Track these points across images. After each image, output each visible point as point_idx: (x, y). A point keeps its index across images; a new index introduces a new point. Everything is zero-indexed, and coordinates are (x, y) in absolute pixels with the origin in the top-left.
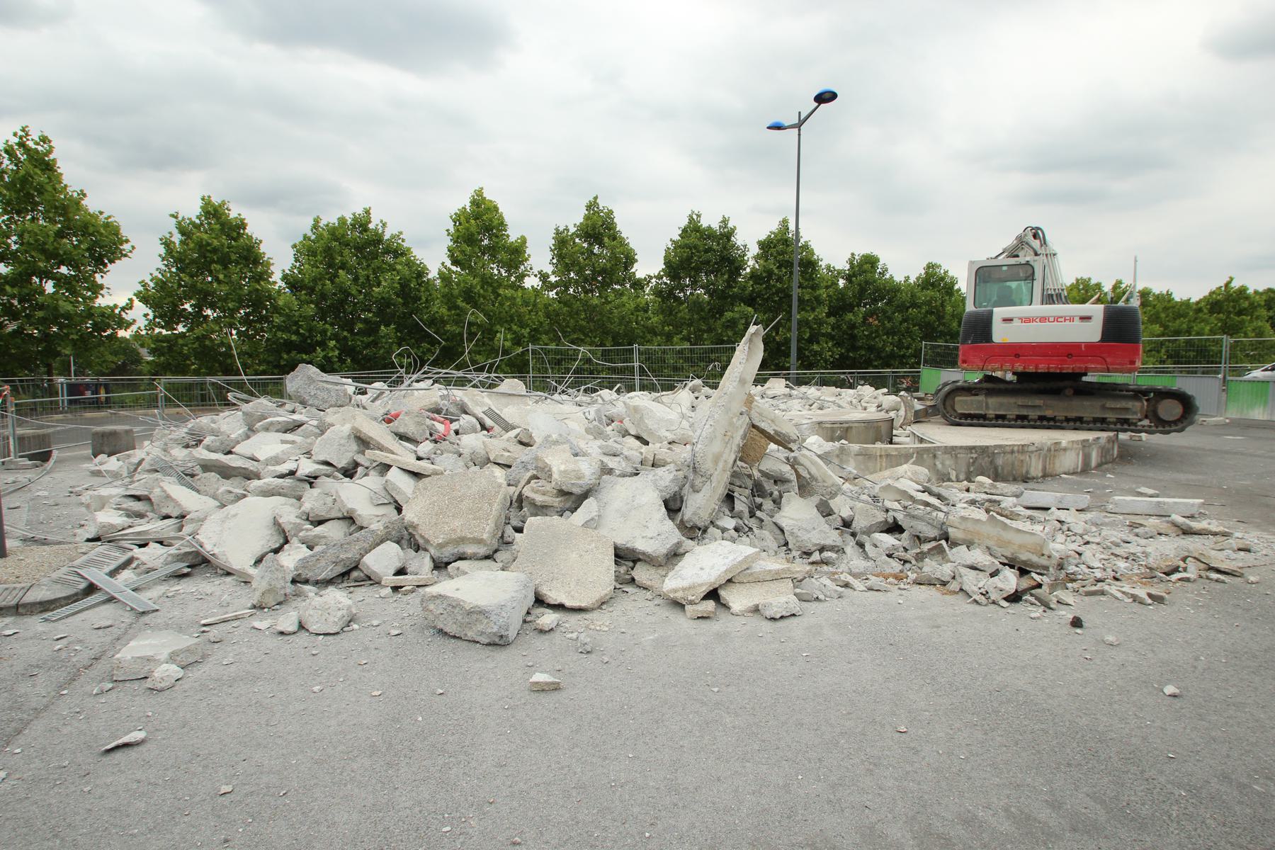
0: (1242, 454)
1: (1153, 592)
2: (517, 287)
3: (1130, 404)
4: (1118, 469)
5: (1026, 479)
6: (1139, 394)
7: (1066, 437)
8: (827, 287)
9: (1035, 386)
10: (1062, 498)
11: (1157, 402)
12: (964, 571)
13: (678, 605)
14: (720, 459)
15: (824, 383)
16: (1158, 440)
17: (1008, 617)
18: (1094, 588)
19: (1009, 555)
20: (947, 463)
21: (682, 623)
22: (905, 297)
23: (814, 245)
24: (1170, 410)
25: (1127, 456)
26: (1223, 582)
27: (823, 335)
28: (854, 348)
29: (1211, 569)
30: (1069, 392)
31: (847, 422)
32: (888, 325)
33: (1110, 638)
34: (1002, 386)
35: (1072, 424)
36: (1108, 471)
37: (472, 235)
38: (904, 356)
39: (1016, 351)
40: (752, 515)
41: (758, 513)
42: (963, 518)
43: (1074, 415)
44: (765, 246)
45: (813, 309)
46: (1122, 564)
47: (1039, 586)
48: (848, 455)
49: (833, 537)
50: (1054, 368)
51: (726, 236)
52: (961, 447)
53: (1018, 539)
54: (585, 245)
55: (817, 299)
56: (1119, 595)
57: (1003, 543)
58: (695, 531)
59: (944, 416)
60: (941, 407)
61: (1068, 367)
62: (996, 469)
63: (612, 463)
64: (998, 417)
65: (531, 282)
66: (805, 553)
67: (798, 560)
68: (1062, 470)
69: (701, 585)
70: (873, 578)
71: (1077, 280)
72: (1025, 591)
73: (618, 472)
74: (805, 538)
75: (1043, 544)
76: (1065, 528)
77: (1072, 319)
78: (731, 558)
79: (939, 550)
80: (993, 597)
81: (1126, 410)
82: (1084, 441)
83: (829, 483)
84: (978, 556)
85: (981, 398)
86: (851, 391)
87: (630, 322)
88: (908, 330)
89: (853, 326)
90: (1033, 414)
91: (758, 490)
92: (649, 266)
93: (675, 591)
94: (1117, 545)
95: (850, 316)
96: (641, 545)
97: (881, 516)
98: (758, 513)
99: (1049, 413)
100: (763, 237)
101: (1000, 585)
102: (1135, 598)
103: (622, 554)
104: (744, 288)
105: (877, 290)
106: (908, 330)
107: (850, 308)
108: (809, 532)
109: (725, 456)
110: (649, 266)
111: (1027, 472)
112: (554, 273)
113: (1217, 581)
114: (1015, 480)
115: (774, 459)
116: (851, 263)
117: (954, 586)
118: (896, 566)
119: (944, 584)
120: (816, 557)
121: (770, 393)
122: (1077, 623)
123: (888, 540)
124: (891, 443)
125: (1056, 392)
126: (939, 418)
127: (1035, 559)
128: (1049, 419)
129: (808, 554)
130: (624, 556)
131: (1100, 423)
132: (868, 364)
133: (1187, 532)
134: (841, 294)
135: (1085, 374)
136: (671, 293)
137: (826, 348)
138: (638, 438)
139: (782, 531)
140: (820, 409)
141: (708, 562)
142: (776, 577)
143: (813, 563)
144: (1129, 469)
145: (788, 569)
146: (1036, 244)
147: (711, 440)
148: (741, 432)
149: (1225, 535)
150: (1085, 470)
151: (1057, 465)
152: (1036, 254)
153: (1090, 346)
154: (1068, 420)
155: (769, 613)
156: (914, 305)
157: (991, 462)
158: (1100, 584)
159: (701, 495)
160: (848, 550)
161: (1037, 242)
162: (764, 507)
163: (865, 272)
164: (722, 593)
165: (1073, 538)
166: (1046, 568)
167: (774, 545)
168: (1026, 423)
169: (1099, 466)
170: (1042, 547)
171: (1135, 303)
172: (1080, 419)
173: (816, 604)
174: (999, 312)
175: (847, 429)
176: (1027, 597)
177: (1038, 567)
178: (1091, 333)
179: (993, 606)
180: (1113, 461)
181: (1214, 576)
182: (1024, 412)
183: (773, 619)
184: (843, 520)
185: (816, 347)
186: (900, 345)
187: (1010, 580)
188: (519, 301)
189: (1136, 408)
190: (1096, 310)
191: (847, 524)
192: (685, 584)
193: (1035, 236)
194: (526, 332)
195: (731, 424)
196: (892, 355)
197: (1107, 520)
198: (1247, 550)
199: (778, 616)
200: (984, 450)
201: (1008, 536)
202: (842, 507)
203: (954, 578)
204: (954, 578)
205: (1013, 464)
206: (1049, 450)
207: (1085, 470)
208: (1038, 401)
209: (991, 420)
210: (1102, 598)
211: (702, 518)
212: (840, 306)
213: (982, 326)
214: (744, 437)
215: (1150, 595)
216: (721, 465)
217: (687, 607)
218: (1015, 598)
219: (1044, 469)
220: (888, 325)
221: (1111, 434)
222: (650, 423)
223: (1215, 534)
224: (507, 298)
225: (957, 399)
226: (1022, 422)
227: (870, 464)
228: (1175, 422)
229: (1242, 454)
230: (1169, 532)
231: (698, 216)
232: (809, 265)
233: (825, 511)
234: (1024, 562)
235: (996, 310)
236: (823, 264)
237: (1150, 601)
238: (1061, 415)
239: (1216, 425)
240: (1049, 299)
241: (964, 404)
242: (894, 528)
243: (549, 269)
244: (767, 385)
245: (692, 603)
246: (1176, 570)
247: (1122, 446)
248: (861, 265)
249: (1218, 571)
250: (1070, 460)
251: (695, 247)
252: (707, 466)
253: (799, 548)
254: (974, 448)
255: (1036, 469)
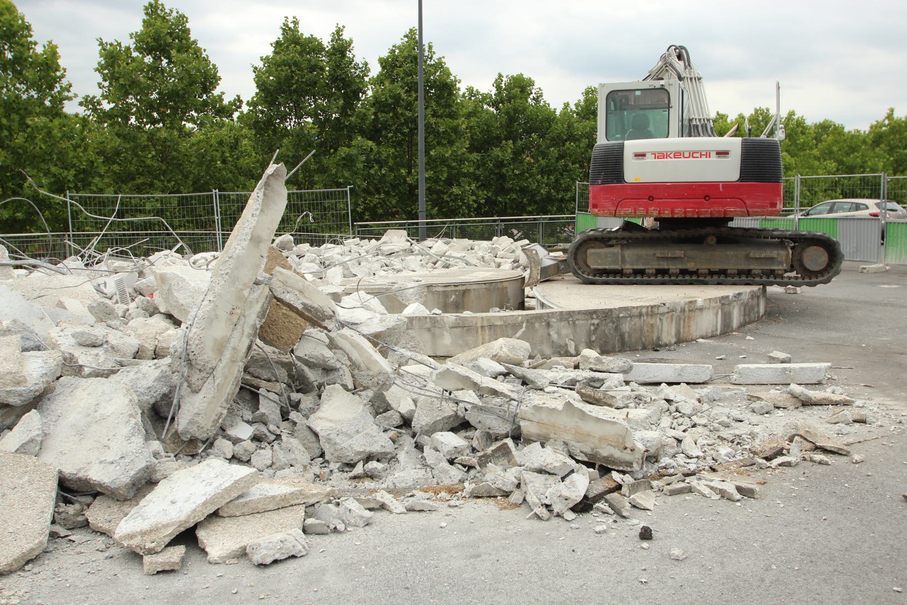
0: (893, 305)
1: (744, 484)
2: (55, 112)
3: (774, 253)
4: (763, 329)
5: (657, 347)
6: (782, 241)
7: (702, 294)
8: (469, 115)
9: (675, 234)
10: (682, 370)
11: (803, 249)
12: (529, 476)
13: (135, 556)
14: (227, 343)
15: (464, 234)
16: (804, 291)
17: (569, 534)
18: (682, 485)
19: (588, 451)
20: (564, 332)
21: (135, 581)
22: (558, 128)
23: (449, 64)
24: (815, 258)
25: (776, 313)
26: (827, 464)
27: (465, 175)
28: (502, 191)
29: (817, 448)
30: (712, 240)
31: (463, 284)
32: (543, 162)
33: (676, 552)
34: (638, 235)
35: (715, 277)
36: (750, 332)
37: (190, 48)
38: (562, 200)
39: (650, 193)
40: (285, 416)
41: (293, 415)
42: (537, 408)
43: (717, 267)
44: (389, 65)
45: (451, 143)
46: (724, 450)
47: (619, 487)
48: (442, 328)
49: (381, 442)
50: (691, 212)
51: (341, 49)
52: (579, 312)
53: (597, 430)
54: (148, 59)
55: (455, 130)
56: (707, 491)
57: (583, 437)
58: (192, 448)
59: (576, 274)
60: (572, 262)
61: (706, 212)
62: (622, 336)
63: (85, 358)
64: (637, 272)
65: (71, 108)
66: (348, 465)
67: (337, 475)
68: (698, 334)
69: (166, 526)
70: (419, 494)
71: (756, 111)
72: (600, 497)
73: (87, 370)
74: (345, 445)
75: (625, 434)
76: (673, 408)
77: (708, 154)
78: (216, 483)
79: (504, 451)
80: (556, 509)
81: (772, 259)
82: (723, 298)
83: (375, 370)
84: (552, 457)
85: (617, 250)
86: (485, 244)
87: (213, 160)
88: (565, 168)
89: (500, 164)
90: (674, 267)
91: (300, 384)
92: (237, 85)
93: (131, 536)
94: (727, 426)
95: (496, 151)
96: (98, 475)
97: (449, 409)
98: (293, 415)
99: (691, 266)
100: (385, 54)
101: (565, 493)
102: (723, 494)
103: (68, 484)
104: (364, 117)
105: (529, 119)
106: (565, 168)
107: (495, 141)
108: (351, 437)
109: (233, 342)
110: (237, 85)
111: (659, 338)
112: (104, 97)
113: (820, 463)
114: (644, 348)
115: (312, 345)
116: (498, 87)
117: (516, 497)
118: (456, 473)
119: (506, 495)
120: (359, 469)
121: (386, 248)
122: (646, 534)
123: (451, 440)
124: (522, 306)
125: (698, 241)
126: (570, 276)
127: (617, 454)
128: (691, 273)
129: (351, 465)
130: (70, 489)
131: (744, 276)
132: (522, 210)
133: (807, 403)
134: (487, 128)
135: (732, 219)
136: (269, 123)
137: (467, 190)
138: (169, 316)
139: (316, 435)
140: (447, 266)
141: (187, 489)
142: (283, 505)
143: (355, 478)
144: (774, 329)
145: (301, 493)
146: (679, 65)
147: (210, 320)
148: (257, 308)
149: (846, 404)
150: (726, 331)
151: (693, 327)
152: (680, 78)
153: (728, 185)
154: (711, 273)
155: (257, 558)
156: (572, 138)
157: (617, 329)
158: (688, 479)
159: (201, 395)
160: (402, 456)
161: (681, 63)
162: (302, 406)
163: (515, 97)
164: (201, 534)
165: (680, 420)
166: (630, 464)
167: (305, 458)
168: (666, 278)
169: (742, 325)
170: (624, 438)
171: (780, 135)
172: (723, 272)
173: (334, 538)
174: (631, 146)
175: (465, 293)
176: (601, 505)
177: (621, 463)
178: (729, 171)
179: (555, 521)
180: (759, 320)
181: (819, 457)
182: (664, 265)
183: (262, 566)
184: (402, 416)
185: (455, 190)
186: (557, 186)
187: (581, 483)
188: (56, 133)
189: (782, 256)
190: (734, 144)
191: (406, 423)
192: (145, 525)
193: (680, 57)
194: (70, 174)
195: (240, 298)
196: (549, 199)
197: (728, 394)
198: (863, 422)
199: (268, 561)
200: (606, 314)
201: (588, 427)
202: (401, 400)
203: (518, 486)
204: (518, 486)
205: (641, 330)
206: (683, 310)
207: (726, 331)
208: (679, 253)
209: (628, 276)
210: (688, 497)
211: (206, 427)
212: (484, 142)
213: (613, 164)
214: (262, 314)
215: (739, 489)
216: (228, 354)
217: (147, 559)
218: (584, 506)
219: (678, 333)
220: (543, 162)
221: (755, 288)
222: (181, 297)
223: (836, 404)
224: (38, 129)
225: (590, 251)
226: (663, 277)
227: (470, 339)
228: (821, 273)
229: (893, 305)
230: (787, 404)
231: (296, 23)
232: (444, 88)
233: (380, 407)
234: (606, 459)
235: (627, 143)
236: (462, 88)
237: (738, 496)
238: (703, 267)
239: (876, 272)
240: (690, 129)
241: (598, 258)
242: (461, 425)
243: (97, 93)
244: (384, 238)
245: (151, 552)
246: (780, 453)
247: (770, 300)
248: (509, 88)
249: (825, 451)
250: (708, 321)
251: (296, 64)
252: (207, 356)
253: (339, 458)
254: (595, 312)
255: (668, 334)
